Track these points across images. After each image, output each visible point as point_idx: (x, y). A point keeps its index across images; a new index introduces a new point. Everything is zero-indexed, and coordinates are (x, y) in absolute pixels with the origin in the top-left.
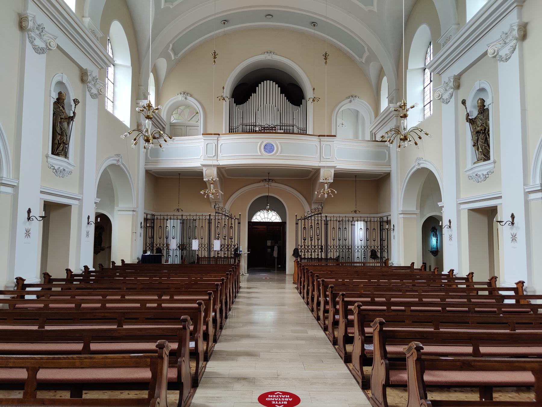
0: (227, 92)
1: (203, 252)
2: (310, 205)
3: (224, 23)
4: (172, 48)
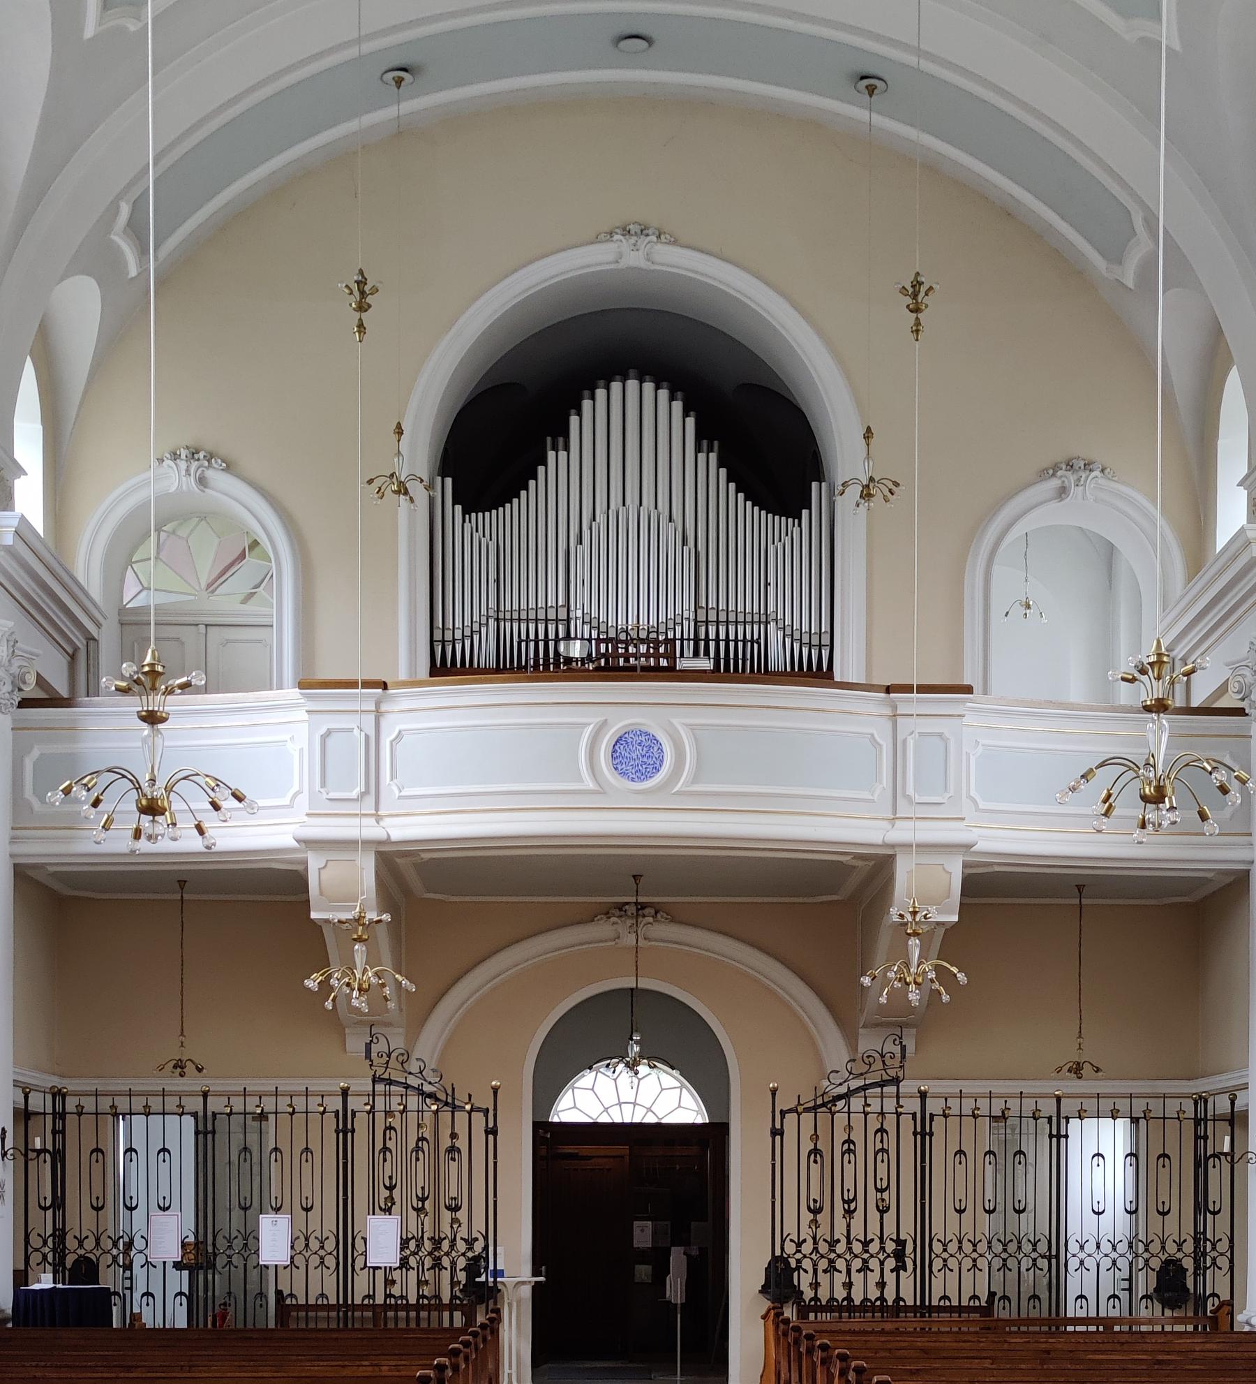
0: (418, 453)
1: (314, 1275)
2: (851, 1039)
3: (399, 82)
4: (130, 223)
